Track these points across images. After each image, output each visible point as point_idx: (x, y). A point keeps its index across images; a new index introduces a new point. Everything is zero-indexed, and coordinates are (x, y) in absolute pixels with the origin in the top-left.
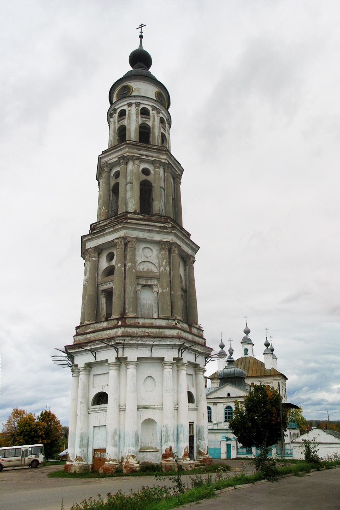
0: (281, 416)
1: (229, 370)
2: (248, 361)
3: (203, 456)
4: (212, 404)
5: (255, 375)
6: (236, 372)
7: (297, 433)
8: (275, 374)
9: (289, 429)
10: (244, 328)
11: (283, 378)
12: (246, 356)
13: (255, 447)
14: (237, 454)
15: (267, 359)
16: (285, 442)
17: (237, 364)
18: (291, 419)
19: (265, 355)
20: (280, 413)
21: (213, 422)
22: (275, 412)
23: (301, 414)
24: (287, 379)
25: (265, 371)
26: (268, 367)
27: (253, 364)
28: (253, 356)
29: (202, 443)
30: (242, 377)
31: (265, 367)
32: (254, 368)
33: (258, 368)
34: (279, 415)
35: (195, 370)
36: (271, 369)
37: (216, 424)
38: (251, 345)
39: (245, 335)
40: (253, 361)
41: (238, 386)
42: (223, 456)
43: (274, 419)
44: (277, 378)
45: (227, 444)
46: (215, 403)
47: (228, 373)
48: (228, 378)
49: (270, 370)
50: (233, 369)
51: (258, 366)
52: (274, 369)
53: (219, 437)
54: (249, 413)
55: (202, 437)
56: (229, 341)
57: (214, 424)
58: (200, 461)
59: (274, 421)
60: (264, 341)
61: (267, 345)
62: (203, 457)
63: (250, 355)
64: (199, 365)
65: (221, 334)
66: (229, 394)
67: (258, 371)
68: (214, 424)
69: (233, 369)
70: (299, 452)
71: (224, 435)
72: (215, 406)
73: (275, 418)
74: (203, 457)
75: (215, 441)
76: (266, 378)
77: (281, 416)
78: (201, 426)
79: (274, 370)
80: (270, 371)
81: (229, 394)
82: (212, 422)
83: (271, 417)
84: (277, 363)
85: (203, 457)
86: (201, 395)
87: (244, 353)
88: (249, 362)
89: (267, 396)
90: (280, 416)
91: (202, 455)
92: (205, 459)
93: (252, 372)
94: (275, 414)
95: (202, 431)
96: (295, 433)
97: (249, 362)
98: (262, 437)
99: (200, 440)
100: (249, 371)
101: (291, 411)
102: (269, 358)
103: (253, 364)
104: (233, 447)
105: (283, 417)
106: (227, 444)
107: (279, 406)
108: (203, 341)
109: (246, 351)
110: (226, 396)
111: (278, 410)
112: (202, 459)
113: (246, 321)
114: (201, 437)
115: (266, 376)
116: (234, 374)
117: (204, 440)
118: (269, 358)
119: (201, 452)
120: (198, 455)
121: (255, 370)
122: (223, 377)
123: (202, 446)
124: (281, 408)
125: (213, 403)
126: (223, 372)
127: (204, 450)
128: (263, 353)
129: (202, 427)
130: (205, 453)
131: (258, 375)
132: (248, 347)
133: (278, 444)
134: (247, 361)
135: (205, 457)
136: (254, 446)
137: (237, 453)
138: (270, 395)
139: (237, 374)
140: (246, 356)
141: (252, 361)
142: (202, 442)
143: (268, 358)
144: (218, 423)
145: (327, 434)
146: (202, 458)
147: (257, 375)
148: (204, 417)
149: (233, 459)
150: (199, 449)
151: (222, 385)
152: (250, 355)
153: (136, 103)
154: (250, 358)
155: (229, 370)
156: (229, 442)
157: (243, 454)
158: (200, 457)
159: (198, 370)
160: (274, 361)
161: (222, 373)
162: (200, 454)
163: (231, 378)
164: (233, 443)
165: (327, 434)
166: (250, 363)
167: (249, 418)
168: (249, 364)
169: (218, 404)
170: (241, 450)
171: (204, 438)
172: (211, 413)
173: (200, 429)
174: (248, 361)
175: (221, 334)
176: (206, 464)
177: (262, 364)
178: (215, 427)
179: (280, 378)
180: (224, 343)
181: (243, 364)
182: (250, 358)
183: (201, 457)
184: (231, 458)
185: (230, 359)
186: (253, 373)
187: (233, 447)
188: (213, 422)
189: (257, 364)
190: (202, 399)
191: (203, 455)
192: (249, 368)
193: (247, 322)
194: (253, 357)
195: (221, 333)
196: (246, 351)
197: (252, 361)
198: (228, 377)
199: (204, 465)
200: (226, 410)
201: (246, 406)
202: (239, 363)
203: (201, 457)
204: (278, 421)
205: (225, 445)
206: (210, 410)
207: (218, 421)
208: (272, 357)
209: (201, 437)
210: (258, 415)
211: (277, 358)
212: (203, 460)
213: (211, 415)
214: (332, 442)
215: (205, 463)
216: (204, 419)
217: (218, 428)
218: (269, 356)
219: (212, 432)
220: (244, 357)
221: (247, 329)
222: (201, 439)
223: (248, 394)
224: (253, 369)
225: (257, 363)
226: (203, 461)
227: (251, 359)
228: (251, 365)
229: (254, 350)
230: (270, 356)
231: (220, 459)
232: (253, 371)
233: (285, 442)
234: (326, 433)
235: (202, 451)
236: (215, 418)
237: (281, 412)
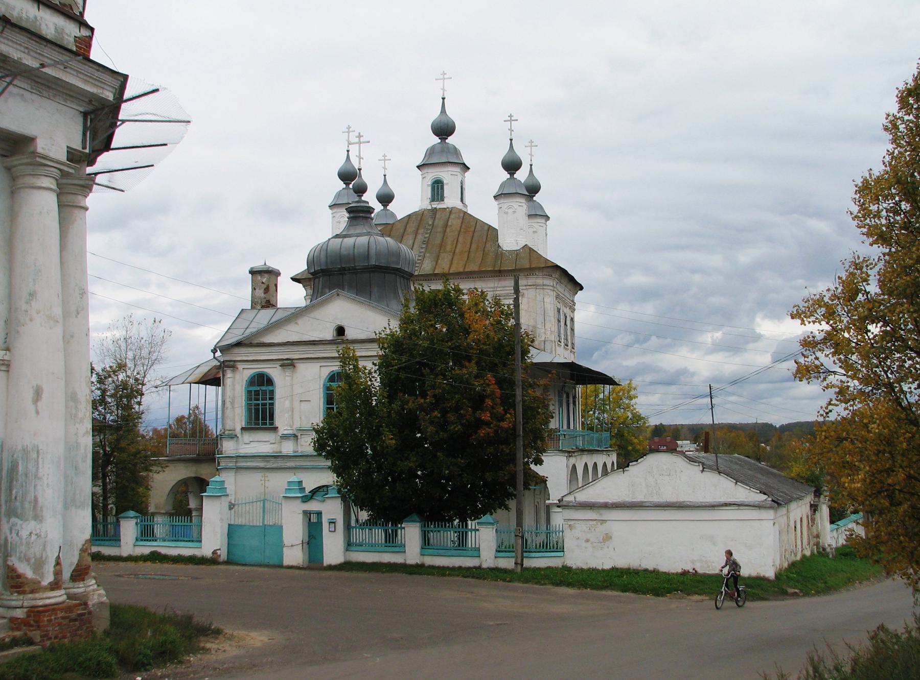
0: (520, 408)
1: (349, 241)
2: (440, 223)
3: (30, 595)
4: (277, 366)
5: (461, 270)
6: (373, 247)
7: (605, 465)
8: (533, 266)
9: (567, 454)
10: (435, 114)
11: (565, 281)
12: (436, 205)
13: (418, 524)
14: (347, 550)
15: (506, 213)
16: (549, 499)
17: (402, 231)
18: (598, 419)
19: (502, 201)
20: (514, 395)
21: (282, 431)
22: (493, 393)
23: (633, 402)
24: (581, 288)
25: (500, 254)
26: (509, 241)
27: (460, 231)
28: (459, 205)
29: (24, 533)
30: (398, 269)
31: (500, 241)
32: (459, 246)
33: (474, 246)
34: (508, 401)
35: (9, 169)
36: (518, 248)
37: (292, 438)
38: (457, 170)
39: (436, 140)
40: (459, 221)
41: (380, 299)
42: (294, 555)
43: (486, 416)
44: (540, 281)
45: (307, 514)
46: (287, 359)
47: (344, 252)
48: (342, 271)
49: (517, 253)
50: (363, 240)
51: (476, 237)
52: (530, 249)
53: (278, 482)
54: (391, 397)
55: (27, 505)
56: (347, 134)
57: (285, 437)
58: (13, 620)
59: (488, 424)
60: (502, 153)
61: (512, 166)
62: (29, 600)
63: (451, 200)
64: (30, 140)
65: (348, 132)
66: (341, 331)
67: (472, 255)
68: (285, 437)
69: (363, 240)
70: (587, 541)
71: (294, 478)
72: (288, 372)
73: (491, 414)
74: (26, 604)
75: (264, 501)
76: (500, 280)
77: (520, 408)
78: (20, 447)
79: (529, 251)
80: (517, 255)
81: (341, 331)
82: (275, 429)
83: (474, 413)
84: (546, 235)
85: (29, 600)
86: (32, 295)
87: (429, 195)
88: (446, 225)
89: (467, 331)
90: (514, 406)
91: (24, 593)
92: (35, 613)
93: (450, 258)
94: (493, 400)
95: (26, 475)
96: (595, 465)
97: (446, 225)
98: (378, 502)
99: (17, 516)
100: (442, 255)
101: (601, 396)
102: (514, 212)
103: (457, 233)
104: (332, 522)
105: (525, 411)
106: (305, 512)
107: (513, 371)
108: (88, 33)
109: (438, 188)
110: (329, 334)
111: (506, 384)
112: (20, 614)
113: (443, 90)
114: (22, 502)
115: (500, 271)
116: (367, 256)
117: (38, 518)
118: (514, 212)
119: (19, 576)
120: (5, 590)
121: (462, 253)
122: (324, 267)
123: (23, 548)
124: (519, 376)
125: (281, 362)
126: (325, 246)
127: (38, 565)
128: (494, 193)
129: (25, 451)
130: (45, 583)
131: (473, 267)
132: (449, 176)
133: (507, 508)
134: (436, 221)
135: (41, 603)
136: (415, 517)
137: (349, 545)
138: (481, 327)
139: (378, 254)
140: (436, 205)
141: (455, 223)
142: (27, 528)
143: (510, 211)
144: (299, 435)
145: (702, 471)
146: (22, 607)
147: (466, 270)
148: (39, 404)
149: (331, 568)
150: (10, 563)
151: (319, 295)
152: (451, 200)
153: (881, 645)
154: (451, 211)
155: (349, 241)
156: (314, 506)
157: (372, 547)
158: (14, 603)
159: (28, 170)
160: (535, 225)
161: (323, 254)
162: (12, 587)
163: (353, 271)
164: (332, 509)
165: (702, 471)
166: (448, 230)
167: (389, 416)
168: (445, 231)
169: (302, 367)
170: (359, 535)
171: (35, 508)
172: (272, 398)
173: (17, 466)
174: (440, 223)
175: (348, 132)
176: (38, 639)
177: (491, 233)
178: (288, 448)
179: (548, 281)
180: (394, 187)
181: (421, 231)
182: (451, 212)
183: (19, 603)
184: (325, 564)
185: (357, 202)
186: (455, 262)
187: (332, 522)
188: (282, 431)
189: (471, 233)
190: (38, 313)
191: (32, 592)
192: (442, 246)
193: (445, 96)
194: (460, 210)
195: (349, 127)
196: (438, 188)
197: (455, 223)
198: (344, 269)
199: (30, 642)
200: (328, 389)
201: (385, 364)
202: (410, 230)
203: (16, 599)
204: (504, 424)
205: (301, 516)
206: (270, 388)
207: (297, 425)
208: (525, 207)
209: (18, 504)
210: (422, 401)
211: (547, 218)
212: (28, 616)
213: (272, 405)
214: (723, 500)
215: (36, 635)
216: (38, 413)
217: (300, 449)
218: (515, 205)
219: (275, 465)
220: (430, 208)
221: (444, 118)
222: (19, 511)
223: (395, 325)
224: (457, 250)
225: (472, 229)
226: (25, 623)
227: (452, 216)
228: (451, 235)
229: (466, 187)
230: (519, 206)
231: (281, 566)
232: (455, 258)
233: (549, 499)
234: (701, 468)
235: (26, 570)
236: (286, 415)
237: (519, 392)
